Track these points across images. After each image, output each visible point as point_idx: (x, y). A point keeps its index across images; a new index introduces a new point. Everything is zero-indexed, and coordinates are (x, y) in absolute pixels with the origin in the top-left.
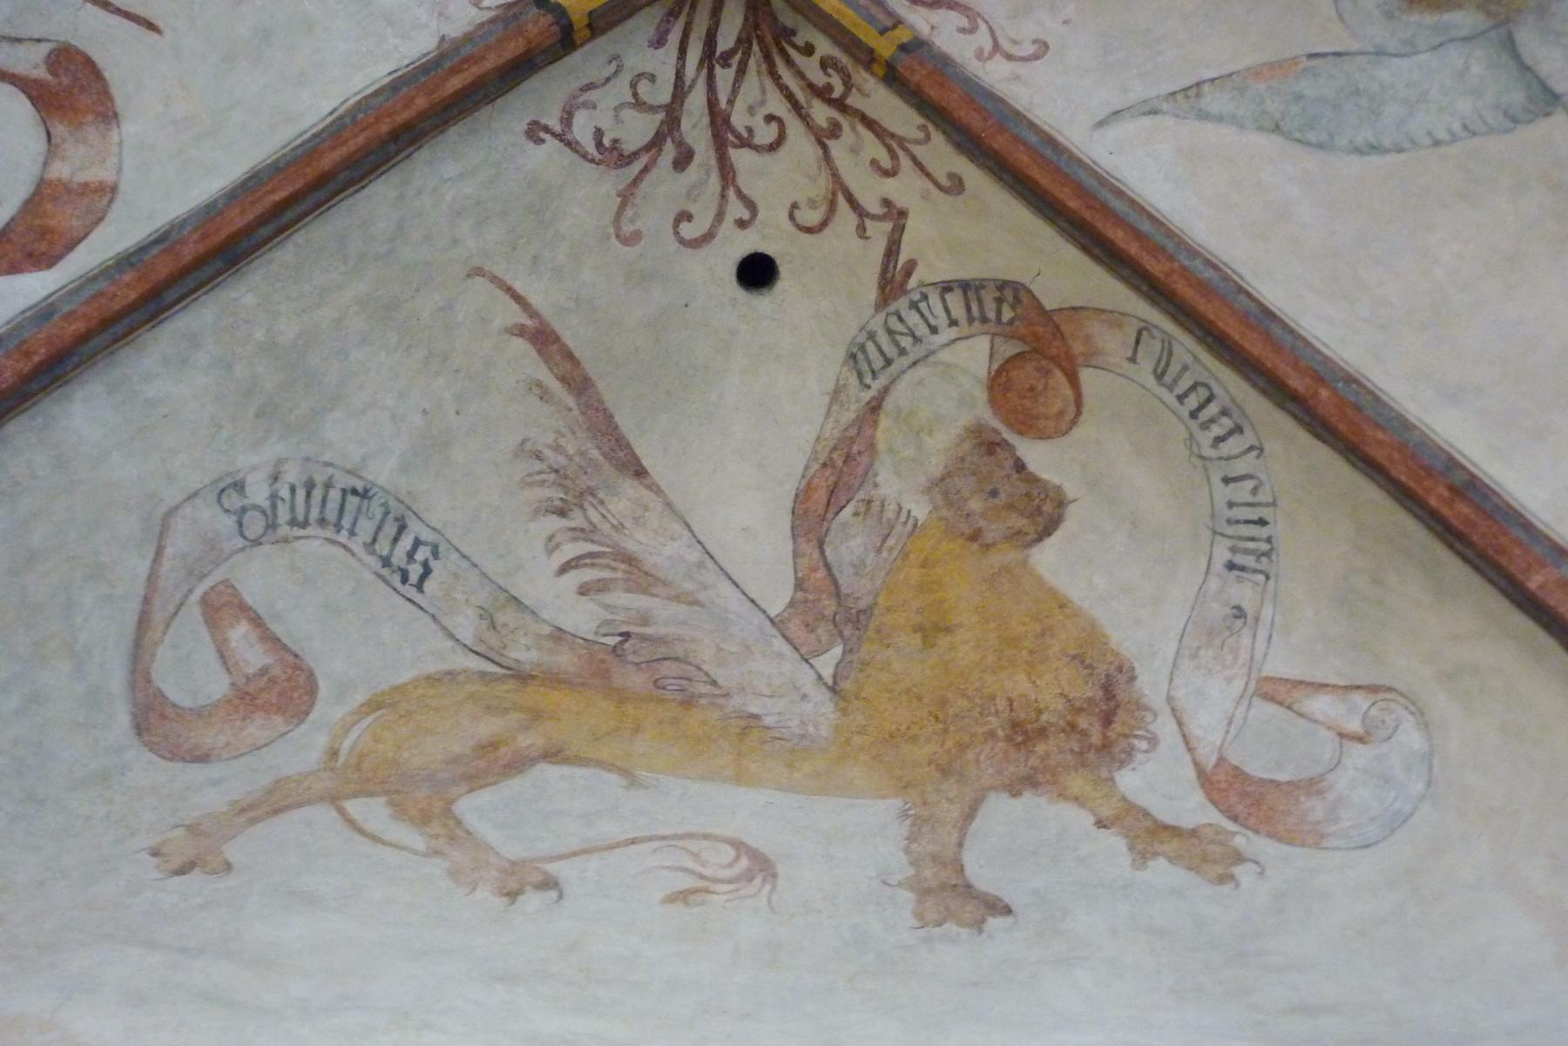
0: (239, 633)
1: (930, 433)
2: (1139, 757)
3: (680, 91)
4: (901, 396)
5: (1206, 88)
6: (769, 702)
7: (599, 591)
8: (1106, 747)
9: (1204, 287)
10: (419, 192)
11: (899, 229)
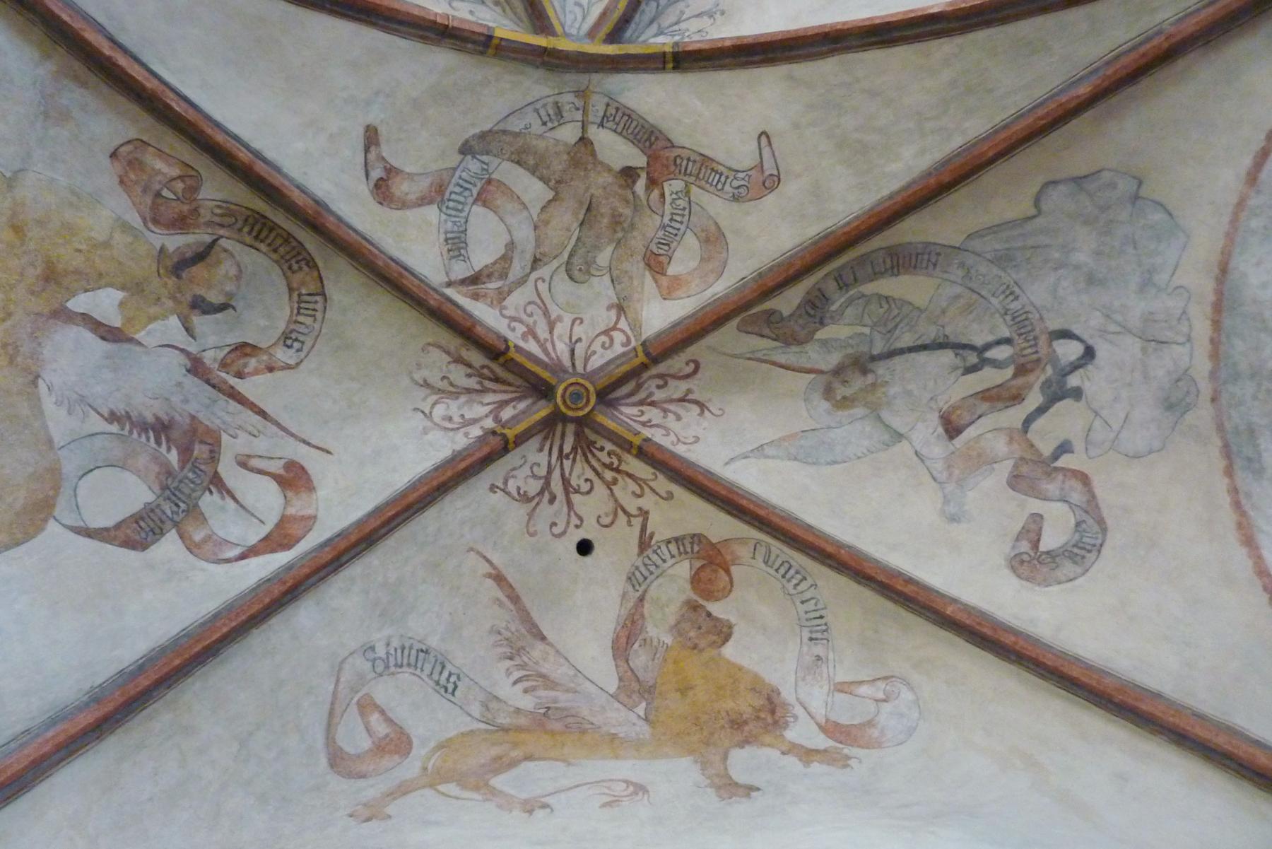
0: (375, 718)
1: (667, 606)
2: (792, 724)
3: (550, 471)
4: (653, 592)
5: (765, 446)
6: (619, 728)
7: (533, 691)
8: (776, 723)
9: (782, 518)
10: (447, 514)
11: (646, 519)
